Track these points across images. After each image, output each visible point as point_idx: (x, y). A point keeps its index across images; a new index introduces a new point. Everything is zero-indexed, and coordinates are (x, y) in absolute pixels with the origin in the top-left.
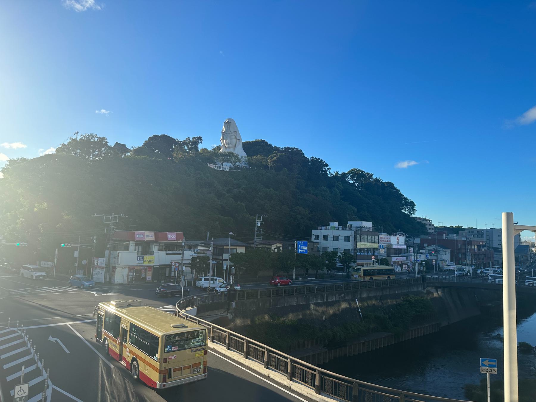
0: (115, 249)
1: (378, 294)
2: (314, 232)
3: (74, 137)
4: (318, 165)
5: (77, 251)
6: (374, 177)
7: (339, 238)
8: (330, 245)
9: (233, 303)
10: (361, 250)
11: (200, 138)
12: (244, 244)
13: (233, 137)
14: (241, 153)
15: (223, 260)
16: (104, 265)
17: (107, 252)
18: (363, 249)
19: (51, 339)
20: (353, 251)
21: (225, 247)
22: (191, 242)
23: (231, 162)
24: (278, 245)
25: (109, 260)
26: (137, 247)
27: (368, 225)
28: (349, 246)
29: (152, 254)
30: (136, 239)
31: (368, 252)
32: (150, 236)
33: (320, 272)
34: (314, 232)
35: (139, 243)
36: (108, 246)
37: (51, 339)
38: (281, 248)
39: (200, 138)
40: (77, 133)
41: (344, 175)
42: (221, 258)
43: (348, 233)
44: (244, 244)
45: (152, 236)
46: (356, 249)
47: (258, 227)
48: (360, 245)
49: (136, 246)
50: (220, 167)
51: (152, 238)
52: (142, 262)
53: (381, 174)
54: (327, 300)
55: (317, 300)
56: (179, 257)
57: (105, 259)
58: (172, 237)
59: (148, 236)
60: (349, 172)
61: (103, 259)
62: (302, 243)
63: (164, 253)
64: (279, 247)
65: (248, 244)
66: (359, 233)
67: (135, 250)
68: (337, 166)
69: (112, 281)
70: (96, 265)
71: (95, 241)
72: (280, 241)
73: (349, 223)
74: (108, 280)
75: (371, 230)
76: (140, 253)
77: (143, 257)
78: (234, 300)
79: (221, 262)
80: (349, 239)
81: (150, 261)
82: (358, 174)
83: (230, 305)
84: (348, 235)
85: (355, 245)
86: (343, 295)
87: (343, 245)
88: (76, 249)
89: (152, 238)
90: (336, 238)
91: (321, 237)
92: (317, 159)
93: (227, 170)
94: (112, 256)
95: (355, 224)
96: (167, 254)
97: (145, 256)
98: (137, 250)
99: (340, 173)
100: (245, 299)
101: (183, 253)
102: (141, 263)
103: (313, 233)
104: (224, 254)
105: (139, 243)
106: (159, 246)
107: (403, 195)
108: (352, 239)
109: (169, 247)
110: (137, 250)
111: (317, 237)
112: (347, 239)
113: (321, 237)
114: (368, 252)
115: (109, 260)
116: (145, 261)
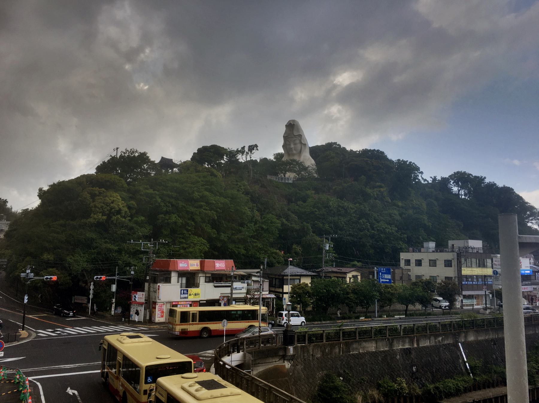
0: (155, 281)
1: (491, 337)
2: (403, 256)
3: (114, 154)
4: (407, 170)
5: (115, 284)
6: (487, 181)
7: (438, 262)
8: (425, 272)
9: (291, 348)
10: (467, 277)
11: (256, 146)
12: (310, 273)
13: (298, 141)
14: (309, 161)
15: (283, 293)
16: (143, 301)
17: (146, 285)
18: (471, 277)
19: (70, 391)
20: (457, 280)
21: (285, 278)
22: (242, 272)
23: (295, 172)
24: (354, 273)
25: (149, 295)
26: (180, 279)
27: (476, 244)
28: (451, 272)
29: (197, 286)
30: (179, 269)
31: (478, 281)
32: (194, 264)
33: (411, 307)
34: (403, 256)
35: (181, 274)
36: (148, 278)
37: (70, 391)
38: (359, 277)
39: (256, 146)
40: (117, 148)
41: (445, 181)
42: (281, 290)
43: (449, 256)
44: (310, 273)
45: (197, 265)
46: (460, 277)
47: (327, 251)
48: (466, 271)
49: (179, 277)
50: (282, 179)
51: (198, 268)
52: (186, 296)
53: (497, 177)
54: (418, 344)
55: (403, 345)
56: (228, 290)
57: (144, 293)
58: (220, 265)
59: (192, 265)
60: (450, 176)
61: (142, 293)
62: (383, 269)
63: (211, 284)
64: (357, 276)
65: (313, 272)
66: (463, 255)
67: (178, 282)
68: (432, 169)
69: (153, 319)
70: (133, 300)
71: (132, 273)
72: (358, 269)
73: (450, 243)
74: (148, 318)
75: (481, 252)
76: (184, 285)
77: (187, 290)
78: (292, 344)
79: (281, 295)
80: (451, 264)
81: (196, 295)
82: (461, 178)
83: (286, 350)
84: (450, 259)
85: (459, 271)
86: (440, 339)
87: (442, 273)
88: (112, 282)
89: (198, 268)
90: (419, 263)
91: (413, 262)
92: (405, 162)
93: (290, 182)
94: (152, 289)
95: (458, 244)
96: (215, 287)
97: (189, 289)
98: (180, 282)
99: (439, 178)
100: (324, 341)
101: (232, 285)
102: (185, 298)
103: (401, 257)
104: (284, 286)
105: (181, 274)
106: (206, 277)
107: (527, 203)
108: (455, 263)
109: (217, 278)
110: (180, 282)
111: (408, 262)
112: (448, 264)
113: (413, 262)
114: (478, 281)
115: (149, 295)
116: (190, 294)
